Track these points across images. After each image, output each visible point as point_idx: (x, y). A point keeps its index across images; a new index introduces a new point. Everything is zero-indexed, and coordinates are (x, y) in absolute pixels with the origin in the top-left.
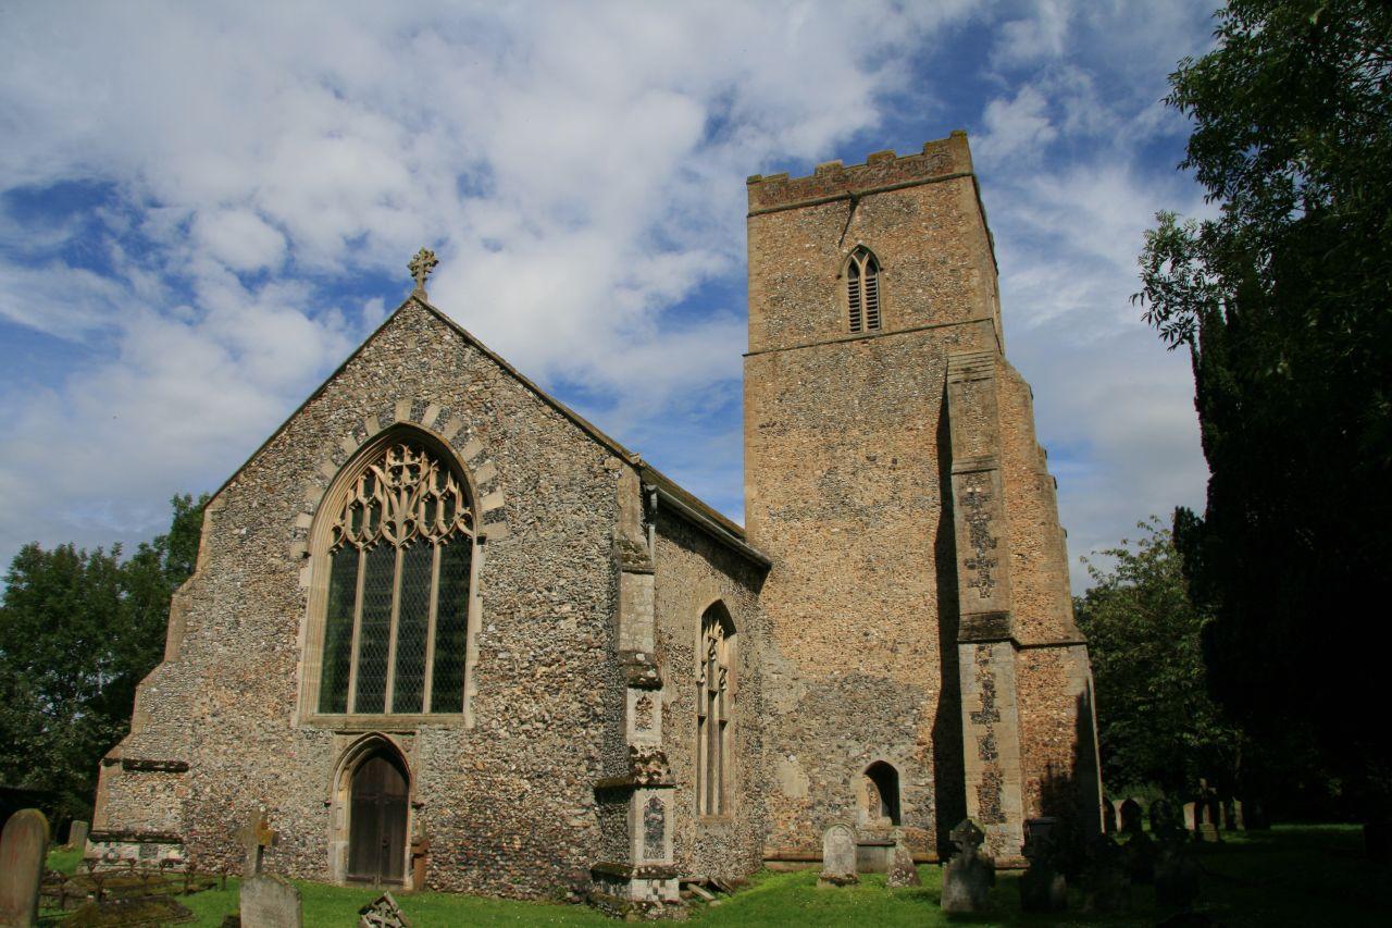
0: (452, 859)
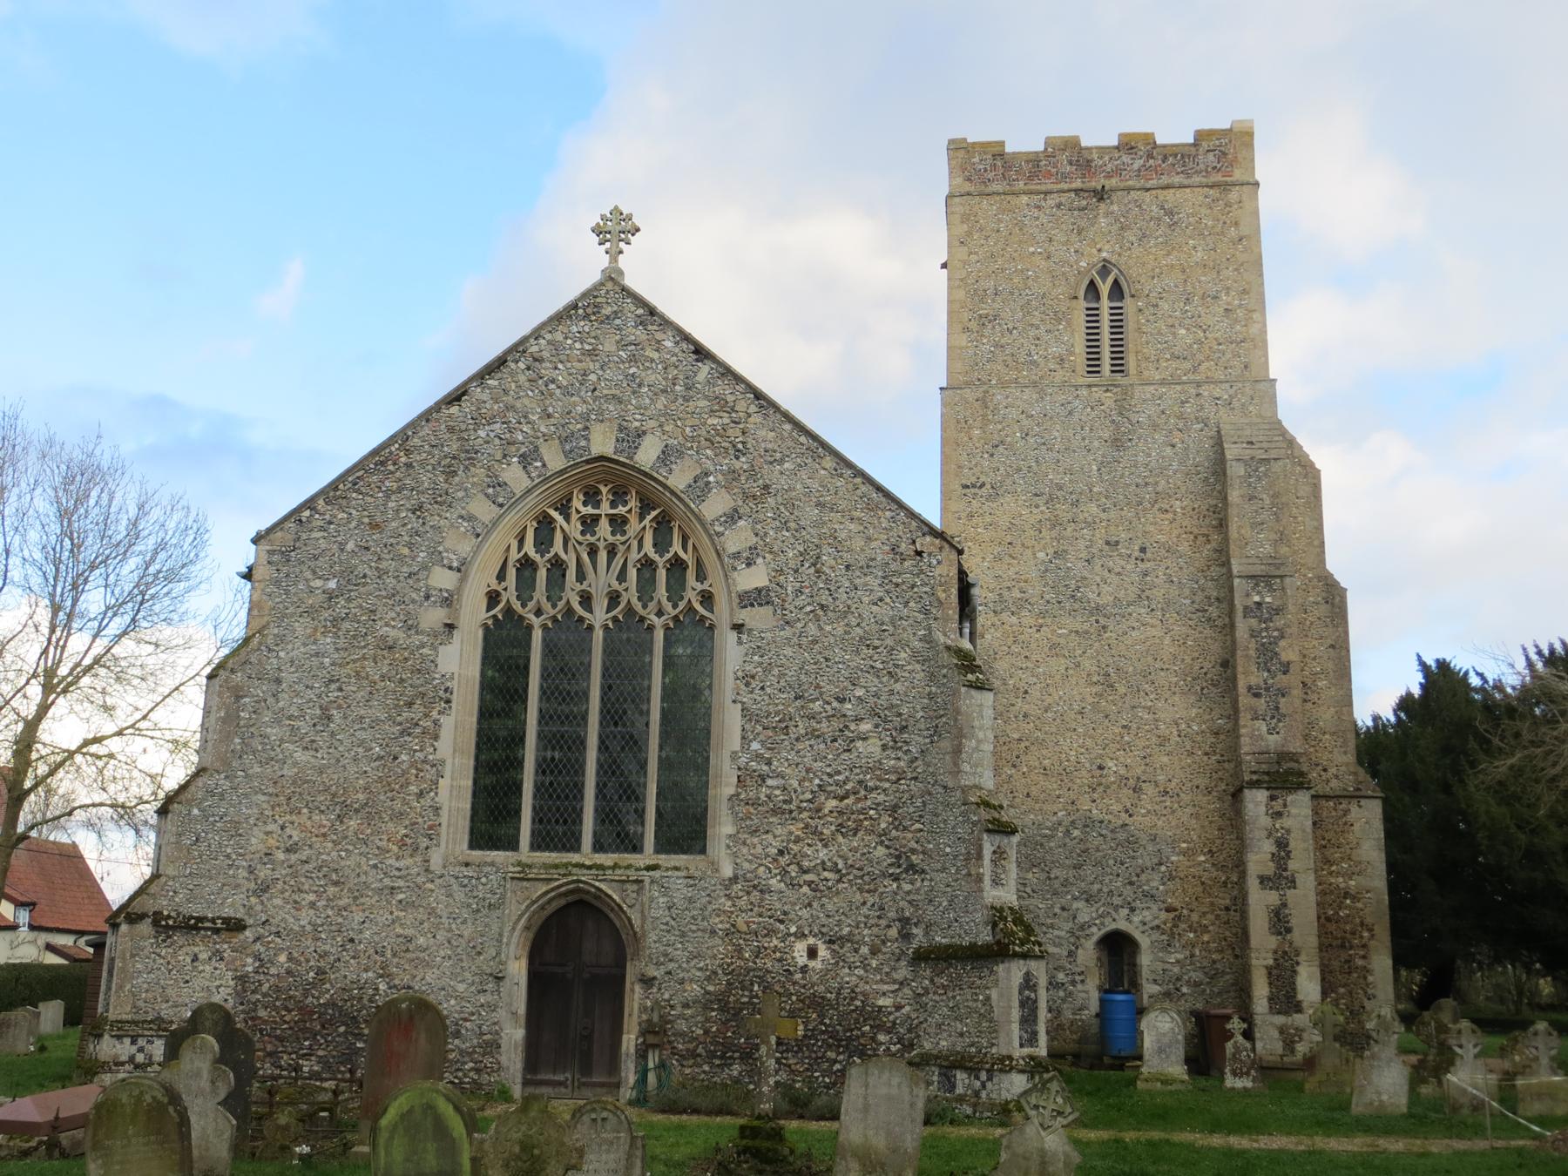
0: (700, 1050)
